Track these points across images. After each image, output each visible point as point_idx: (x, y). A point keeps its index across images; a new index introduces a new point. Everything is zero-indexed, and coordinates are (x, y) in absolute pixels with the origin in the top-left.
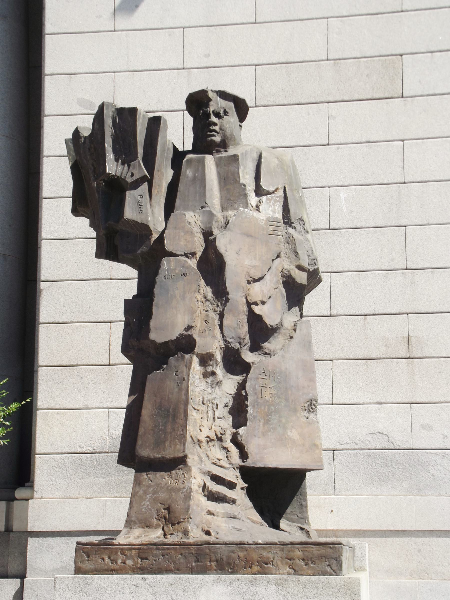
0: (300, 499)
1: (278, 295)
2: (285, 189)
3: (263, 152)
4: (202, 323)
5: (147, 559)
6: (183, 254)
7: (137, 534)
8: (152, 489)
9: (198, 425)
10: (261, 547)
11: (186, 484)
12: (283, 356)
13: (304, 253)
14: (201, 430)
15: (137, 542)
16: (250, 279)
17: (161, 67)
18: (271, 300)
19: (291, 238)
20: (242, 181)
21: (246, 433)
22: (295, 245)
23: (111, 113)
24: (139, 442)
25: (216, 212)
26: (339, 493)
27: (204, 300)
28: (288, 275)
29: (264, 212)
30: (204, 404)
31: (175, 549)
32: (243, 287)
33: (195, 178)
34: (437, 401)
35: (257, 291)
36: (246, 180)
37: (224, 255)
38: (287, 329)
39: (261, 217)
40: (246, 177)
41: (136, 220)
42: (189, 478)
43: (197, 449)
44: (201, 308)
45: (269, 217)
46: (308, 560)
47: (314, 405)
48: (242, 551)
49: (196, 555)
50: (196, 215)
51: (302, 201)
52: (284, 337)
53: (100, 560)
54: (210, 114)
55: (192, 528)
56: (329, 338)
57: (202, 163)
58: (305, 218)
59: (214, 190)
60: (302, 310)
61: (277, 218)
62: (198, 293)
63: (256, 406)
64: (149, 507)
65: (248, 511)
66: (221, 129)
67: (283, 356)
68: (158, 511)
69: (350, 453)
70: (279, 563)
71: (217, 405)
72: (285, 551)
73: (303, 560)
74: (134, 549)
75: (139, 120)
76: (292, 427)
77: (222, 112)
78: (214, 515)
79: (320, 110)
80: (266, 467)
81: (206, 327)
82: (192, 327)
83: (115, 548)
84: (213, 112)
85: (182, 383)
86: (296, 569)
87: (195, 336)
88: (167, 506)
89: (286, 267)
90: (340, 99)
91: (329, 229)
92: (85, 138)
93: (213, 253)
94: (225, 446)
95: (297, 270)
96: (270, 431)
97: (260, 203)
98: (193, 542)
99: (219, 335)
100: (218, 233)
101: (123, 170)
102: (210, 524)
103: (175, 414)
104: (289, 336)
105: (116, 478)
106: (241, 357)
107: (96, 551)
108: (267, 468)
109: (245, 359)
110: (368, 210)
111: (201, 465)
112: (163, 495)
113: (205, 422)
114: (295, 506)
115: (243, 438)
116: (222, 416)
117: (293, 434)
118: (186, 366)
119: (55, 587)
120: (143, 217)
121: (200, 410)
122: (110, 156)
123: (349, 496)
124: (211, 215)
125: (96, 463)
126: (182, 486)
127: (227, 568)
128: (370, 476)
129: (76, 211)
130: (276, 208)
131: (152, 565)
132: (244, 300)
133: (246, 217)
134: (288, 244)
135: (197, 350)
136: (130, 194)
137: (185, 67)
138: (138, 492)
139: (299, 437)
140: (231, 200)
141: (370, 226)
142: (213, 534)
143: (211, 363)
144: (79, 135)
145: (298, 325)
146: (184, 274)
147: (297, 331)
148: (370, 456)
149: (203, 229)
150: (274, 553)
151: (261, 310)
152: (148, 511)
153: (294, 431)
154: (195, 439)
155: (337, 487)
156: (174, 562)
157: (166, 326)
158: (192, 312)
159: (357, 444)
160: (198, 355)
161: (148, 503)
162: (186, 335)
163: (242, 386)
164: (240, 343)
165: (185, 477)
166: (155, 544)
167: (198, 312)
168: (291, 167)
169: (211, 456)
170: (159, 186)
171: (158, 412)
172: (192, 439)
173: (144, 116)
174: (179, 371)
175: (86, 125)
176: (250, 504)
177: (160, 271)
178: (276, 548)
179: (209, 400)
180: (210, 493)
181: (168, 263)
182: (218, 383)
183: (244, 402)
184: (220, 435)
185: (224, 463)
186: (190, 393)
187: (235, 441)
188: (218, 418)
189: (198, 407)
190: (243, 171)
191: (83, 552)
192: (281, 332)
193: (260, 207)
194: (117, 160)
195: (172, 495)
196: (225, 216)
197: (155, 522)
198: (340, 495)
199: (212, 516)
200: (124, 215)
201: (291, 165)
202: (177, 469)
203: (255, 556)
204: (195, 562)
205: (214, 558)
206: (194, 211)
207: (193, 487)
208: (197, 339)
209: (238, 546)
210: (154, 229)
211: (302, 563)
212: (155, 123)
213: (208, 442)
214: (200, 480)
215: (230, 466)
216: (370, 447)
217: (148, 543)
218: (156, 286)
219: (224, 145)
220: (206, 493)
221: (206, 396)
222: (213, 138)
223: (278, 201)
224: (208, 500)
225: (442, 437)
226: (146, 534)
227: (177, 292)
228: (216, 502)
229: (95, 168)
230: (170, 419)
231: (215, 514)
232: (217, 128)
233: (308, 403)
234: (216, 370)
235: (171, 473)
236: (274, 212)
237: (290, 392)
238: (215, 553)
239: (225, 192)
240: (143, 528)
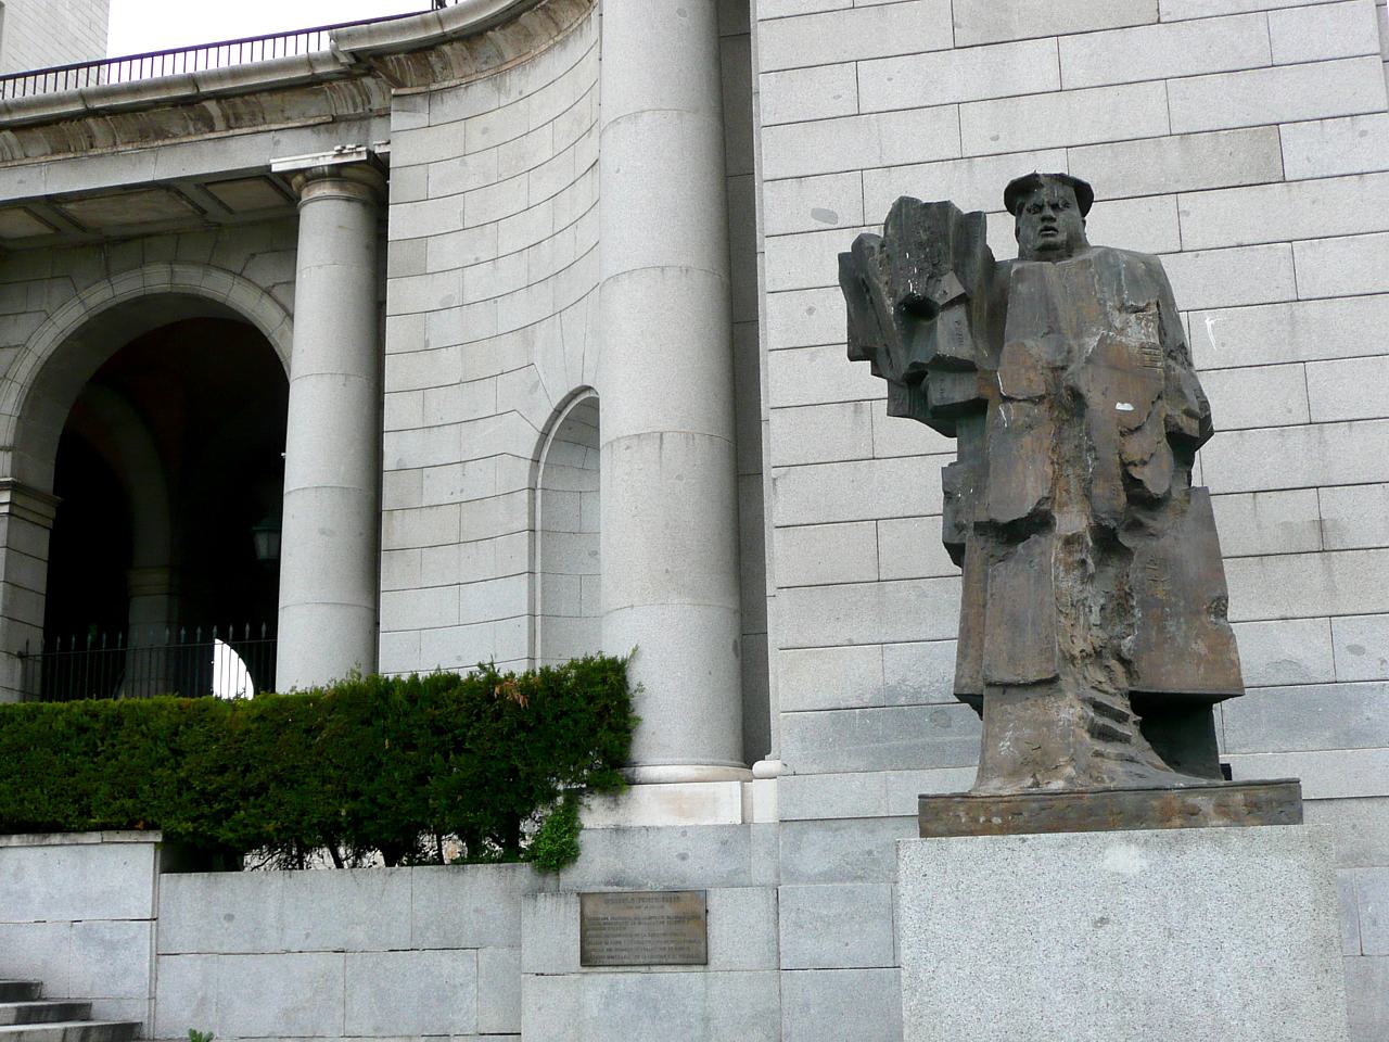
14: (1073, 642)
18: (1154, 458)
34: (1369, 612)
35: (1135, 448)
80: (1165, 692)
84: (1048, 202)
95: (1184, 417)
119: (898, 855)
147: (1192, 503)
153: (1199, 641)
169: (1089, 678)
176: (1147, 744)
213: (1083, 658)
225: (1379, 662)
226: (1228, 665)
236: (1148, 336)
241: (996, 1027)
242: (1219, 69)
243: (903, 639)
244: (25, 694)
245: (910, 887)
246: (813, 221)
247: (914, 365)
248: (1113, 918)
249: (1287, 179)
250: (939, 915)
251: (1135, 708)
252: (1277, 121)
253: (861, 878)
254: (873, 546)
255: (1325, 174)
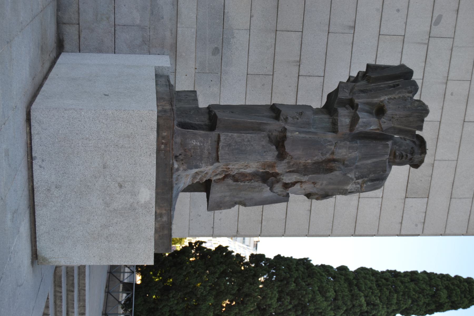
241: (80, 145)
242: (456, 179)
243: (251, 38)
245: (137, 115)
246: (437, 15)
247: (357, 105)
248: (122, 190)
249: (407, 199)
250: (125, 126)
252: (430, 198)
253: (152, 13)
254: (291, 29)
255: (405, 212)
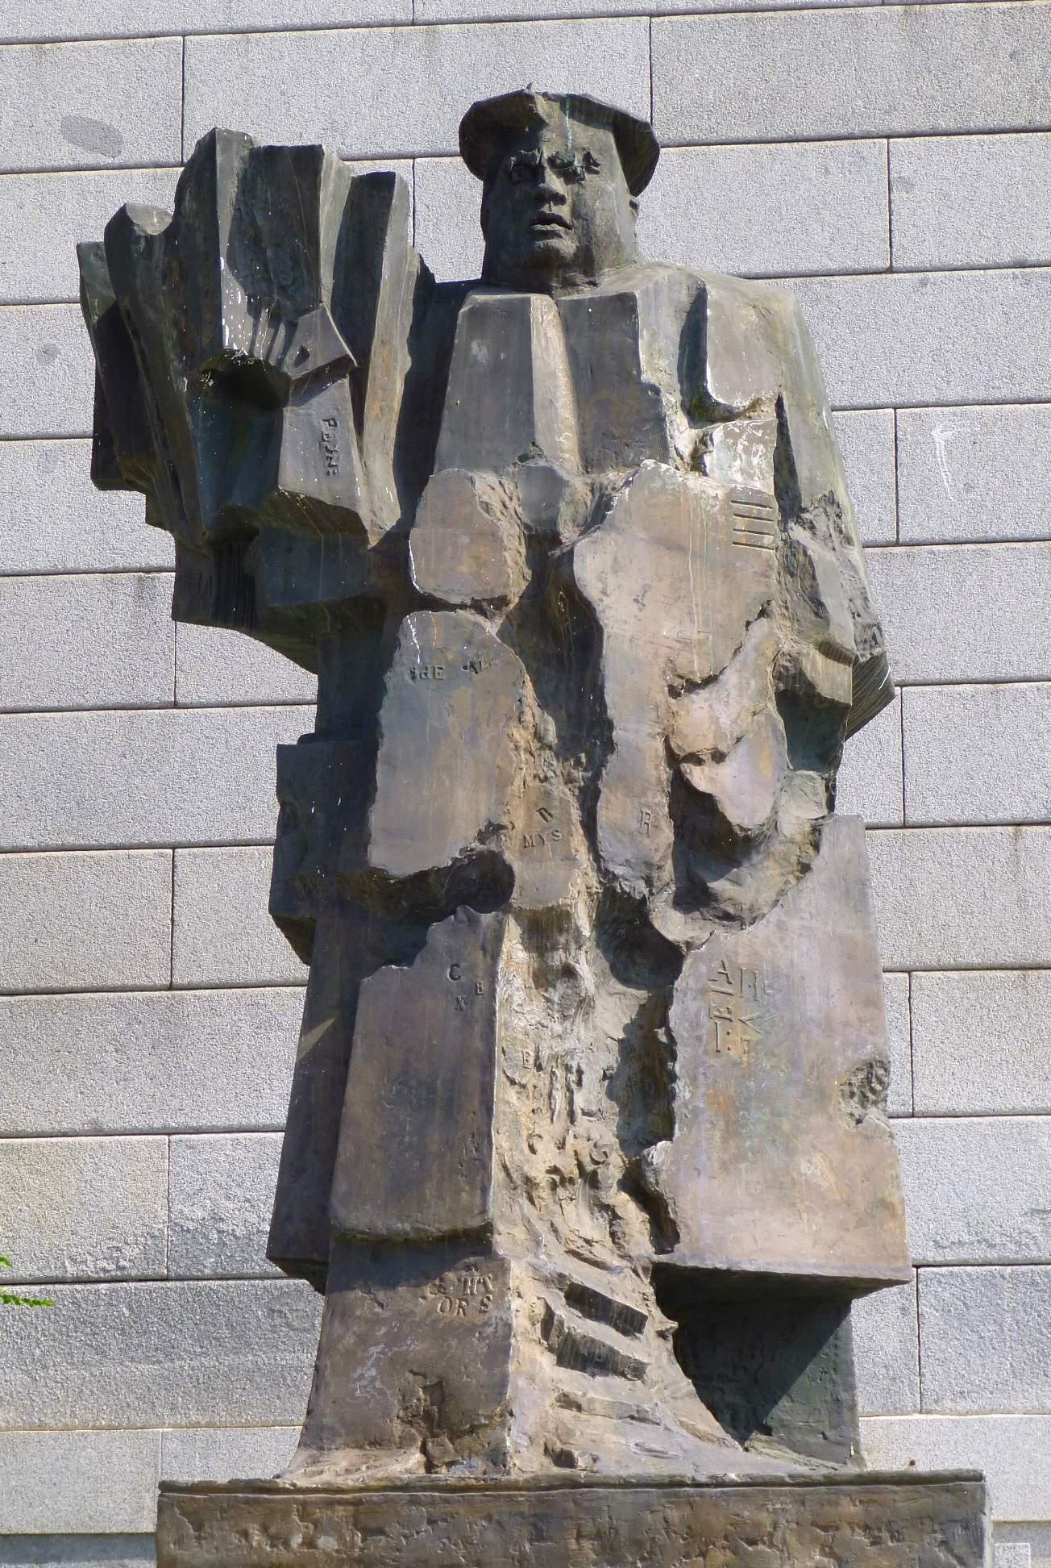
0: (834, 1382)
1: (764, 733)
2: (779, 405)
3: (708, 287)
4: (530, 817)
5: (381, 1531)
6: (469, 602)
7: (344, 1464)
8: (383, 1330)
9: (525, 1133)
10: (736, 1494)
11: (493, 1312)
12: (781, 926)
13: (841, 605)
14: (532, 1150)
15: (350, 1481)
16: (677, 682)
17: (340, 19)
18: (742, 749)
19: (801, 558)
20: (647, 377)
21: (672, 1163)
22: (814, 578)
23: (237, 165)
24: (341, 1185)
25: (568, 473)
26: (934, 1407)
27: (534, 745)
28: (792, 671)
29: (717, 474)
30: (539, 1067)
31: (470, 1502)
32: (657, 707)
33: (497, 368)
35: (704, 718)
36: (660, 375)
37: (599, 608)
38: (792, 841)
39: (708, 488)
40: (657, 364)
41: (316, 496)
42: (502, 1295)
43: (521, 1208)
44: (527, 772)
45: (734, 490)
46: (879, 1530)
47: (881, 1082)
48: (678, 1505)
49: (532, 1520)
50: (505, 481)
51: (832, 444)
52: (782, 867)
53: (235, 1539)
54: (543, 168)
55: (515, 1443)
56: (900, 899)
57: (520, 320)
58: (841, 496)
59: (559, 405)
60: (834, 787)
61: (759, 492)
62: (516, 723)
63: (701, 1078)
64: (378, 1384)
65: (680, 1404)
66: (575, 213)
67: (781, 926)
68: (404, 1397)
69: (969, 1275)
70: (792, 1540)
71: (580, 1072)
72: (808, 1504)
73: (866, 1528)
74: (340, 1502)
75: (327, 186)
76: (814, 1147)
77: (577, 163)
78: (579, 1408)
79: (863, 158)
80: (734, 1269)
81: (544, 829)
82: (501, 827)
83: (281, 1501)
85: (473, 1002)
86: (845, 1555)
87: (508, 857)
88: (435, 1380)
89: (786, 648)
90: (926, 128)
91: (897, 544)
92: (150, 239)
93: (562, 599)
94: (607, 1201)
95: (820, 659)
96: (744, 1158)
97: (705, 444)
98: (526, 1481)
99: (584, 856)
100: (575, 537)
101: (273, 341)
102: (570, 1433)
103: (454, 1095)
104: (799, 863)
105: (195, 1363)
106: (652, 927)
107: (223, 1511)
108: (736, 1273)
109: (663, 932)
110: (1025, 483)
111: (536, 1256)
112: (417, 1347)
113: (544, 1126)
114: (818, 1405)
115: (663, 1177)
116: (594, 1108)
117: (814, 1168)
118: (484, 948)
120: (339, 486)
121: (530, 1087)
122: (234, 297)
123: (967, 1413)
124: (552, 482)
125: (127, 1313)
126: (479, 1319)
127: (630, 1559)
128: (1034, 1350)
129: (107, 472)
130: (755, 461)
131: (398, 1550)
132: (659, 744)
133: (663, 489)
134: (792, 575)
135: (515, 898)
136: (297, 415)
137: (419, 17)
138: (341, 1338)
139: (832, 1178)
140: (614, 437)
141: (1028, 535)
142: (581, 1463)
143: (562, 940)
144: (133, 231)
145: (826, 830)
146: (472, 666)
147: (824, 849)
148: (1034, 1283)
149: (527, 527)
150: (775, 1511)
151: (712, 780)
152: (373, 1396)
153: (817, 1158)
154: (514, 1176)
155: (929, 1385)
156: (467, 1542)
157: (421, 820)
158: (500, 782)
159: (994, 1246)
160: (519, 915)
161: (373, 1372)
162: (481, 854)
163: (655, 1014)
164: (649, 881)
165: (487, 1291)
166: (405, 1488)
167: (518, 782)
168: (797, 334)
170: (384, 391)
171: (399, 1092)
172: (508, 1175)
173: (339, 172)
174: (463, 964)
175: (154, 199)
176: (687, 1385)
177: (397, 654)
178: (779, 1495)
179: (555, 1057)
180: (566, 1340)
181: (423, 629)
182: (581, 1002)
183: (663, 1064)
184: (590, 1167)
185: (604, 1252)
186: (500, 1032)
187: (637, 1184)
188: (584, 1113)
189: (522, 1077)
190: (650, 345)
191: (183, 1514)
192: (772, 849)
193: (707, 459)
194: (254, 310)
195: (449, 1346)
196: (597, 485)
197: (397, 1428)
198: (938, 1413)
199: (574, 1412)
200: (280, 480)
201: (796, 328)
202: (459, 1265)
203: (718, 1522)
204: (531, 1541)
205: (589, 1528)
206: (496, 470)
207: (514, 1323)
208: (517, 867)
209: (667, 1490)
210: (373, 524)
211: (860, 1537)
212: (374, 195)
213: (554, 1186)
214: (535, 1300)
215: (625, 1263)
216: (1035, 1254)
217: (383, 1483)
218: (386, 702)
219: (586, 262)
220: (555, 1340)
221: (548, 1039)
222: (554, 242)
223: (760, 441)
224: (560, 1362)
227: (451, 719)
228: (583, 1370)
229: (182, 335)
230: (438, 1112)
231: (584, 1406)
232: (564, 211)
233: (861, 1076)
234: (577, 962)
235: (442, 1280)
236: (747, 473)
237: (803, 1038)
238: (593, 1512)
239: (595, 411)
240: (361, 1447)
244: (645, 1158)
246: (67, 147)
251: (665, 1303)
